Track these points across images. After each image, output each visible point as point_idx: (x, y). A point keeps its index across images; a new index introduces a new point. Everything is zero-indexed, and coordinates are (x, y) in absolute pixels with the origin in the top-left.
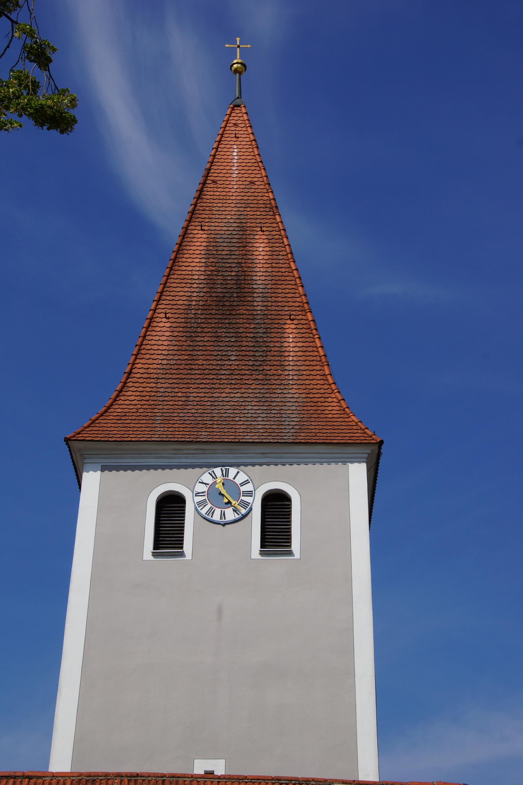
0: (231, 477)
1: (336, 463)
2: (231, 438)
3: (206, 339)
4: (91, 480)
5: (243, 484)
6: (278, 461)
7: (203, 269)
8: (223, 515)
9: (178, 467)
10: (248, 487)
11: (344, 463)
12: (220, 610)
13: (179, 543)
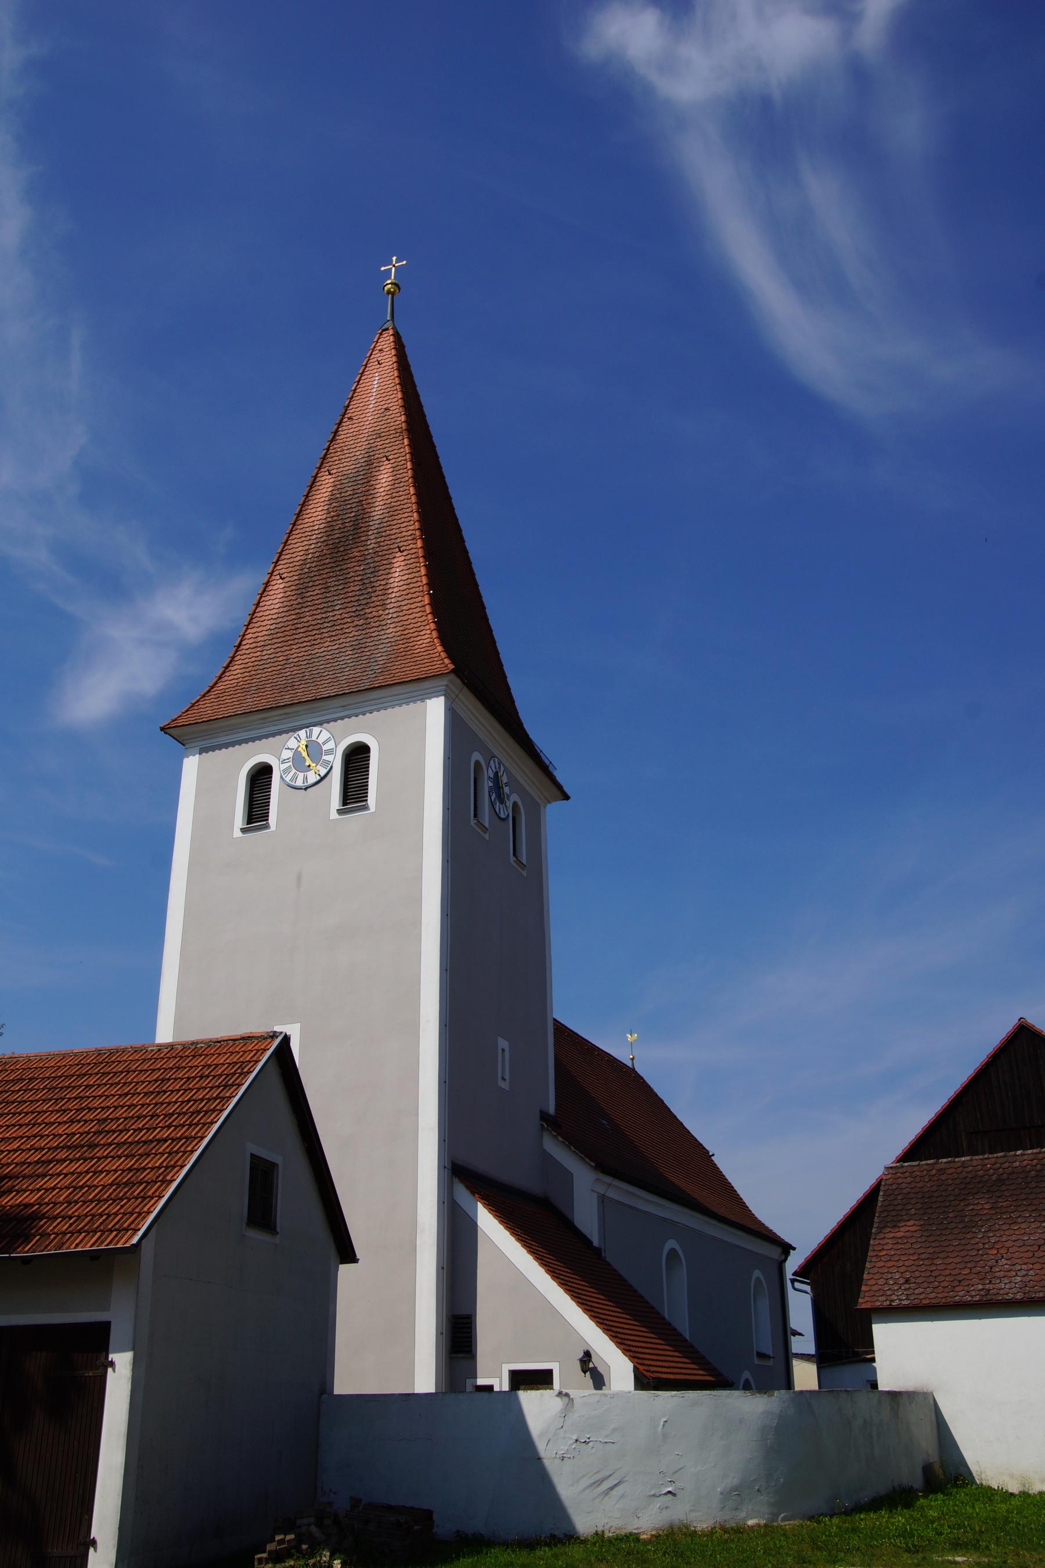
0: (314, 738)
1: (415, 702)
2: (310, 697)
3: (315, 593)
4: (191, 765)
5: (324, 743)
6: (357, 711)
7: (324, 517)
8: (306, 779)
9: (267, 737)
10: (331, 745)
11: (423, 700)
12: (299, 878)
13: (265, 816)
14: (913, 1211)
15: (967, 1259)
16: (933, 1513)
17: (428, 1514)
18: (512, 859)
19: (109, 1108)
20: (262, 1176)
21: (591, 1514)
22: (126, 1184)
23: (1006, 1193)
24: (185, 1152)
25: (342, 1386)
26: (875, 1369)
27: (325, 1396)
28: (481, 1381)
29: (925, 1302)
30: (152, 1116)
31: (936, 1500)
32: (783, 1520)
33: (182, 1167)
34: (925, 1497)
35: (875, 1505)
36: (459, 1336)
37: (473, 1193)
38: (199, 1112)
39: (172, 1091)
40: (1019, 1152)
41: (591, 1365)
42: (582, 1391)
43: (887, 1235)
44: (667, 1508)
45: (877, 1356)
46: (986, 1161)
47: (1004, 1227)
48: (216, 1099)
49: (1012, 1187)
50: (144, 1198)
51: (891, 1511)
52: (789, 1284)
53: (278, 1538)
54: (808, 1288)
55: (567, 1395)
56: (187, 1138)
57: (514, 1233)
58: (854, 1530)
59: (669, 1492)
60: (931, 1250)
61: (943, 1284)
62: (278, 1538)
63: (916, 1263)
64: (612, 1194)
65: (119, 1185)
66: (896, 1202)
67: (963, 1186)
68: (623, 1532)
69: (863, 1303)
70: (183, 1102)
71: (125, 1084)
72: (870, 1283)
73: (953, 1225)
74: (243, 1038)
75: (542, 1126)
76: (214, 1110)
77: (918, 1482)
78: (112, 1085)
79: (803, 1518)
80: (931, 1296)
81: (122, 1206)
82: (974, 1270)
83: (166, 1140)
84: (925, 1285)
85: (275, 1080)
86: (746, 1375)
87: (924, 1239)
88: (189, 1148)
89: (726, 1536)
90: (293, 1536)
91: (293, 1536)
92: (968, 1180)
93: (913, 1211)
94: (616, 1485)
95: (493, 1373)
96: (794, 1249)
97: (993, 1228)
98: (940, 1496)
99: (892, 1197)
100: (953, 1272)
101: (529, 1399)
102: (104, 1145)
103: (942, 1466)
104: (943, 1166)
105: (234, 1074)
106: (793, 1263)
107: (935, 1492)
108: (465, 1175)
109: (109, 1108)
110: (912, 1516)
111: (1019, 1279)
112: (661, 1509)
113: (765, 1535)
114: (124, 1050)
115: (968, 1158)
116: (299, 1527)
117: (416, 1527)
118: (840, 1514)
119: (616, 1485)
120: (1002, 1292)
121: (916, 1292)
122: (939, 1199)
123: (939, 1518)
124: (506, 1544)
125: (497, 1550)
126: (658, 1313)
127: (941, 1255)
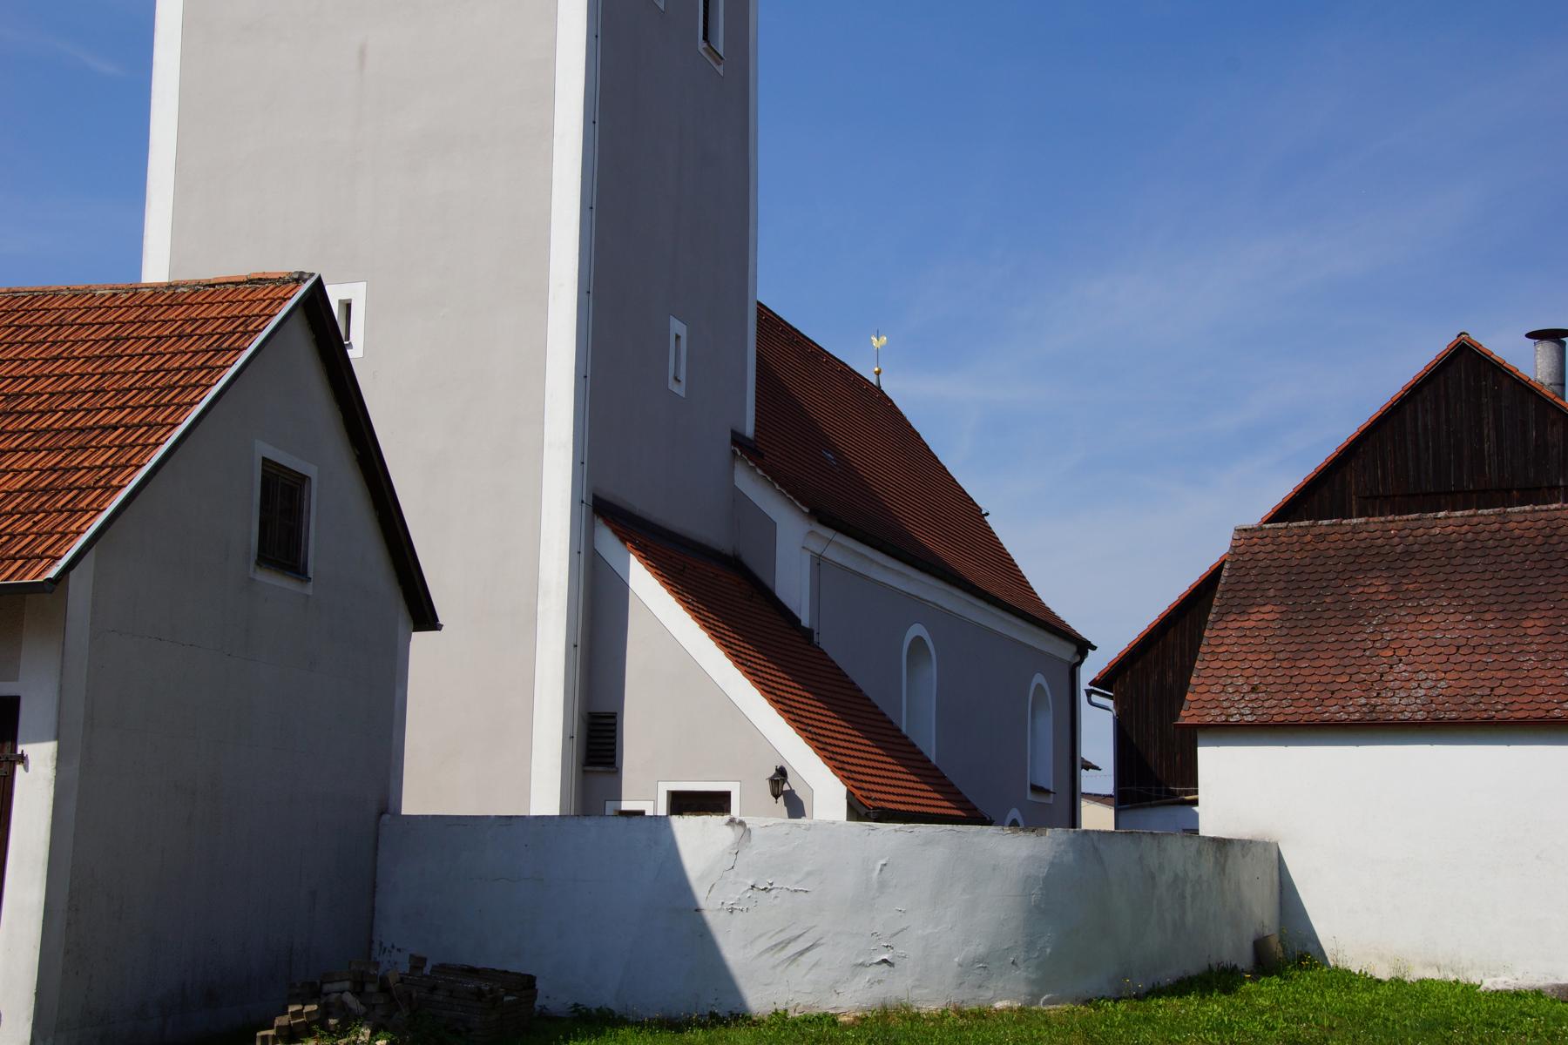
12: (362, 53)
14: (1271, 593)
15: (1346, 662)
16: (1263, 1002)
17: (528, 982)
18: (701, 45)
19: (24, 377)
20: (283, 498)
21: (768, 987)
22: (45, 490)
23: (1415, 572)
24: (145, 446)
25: (416, 800)
26: (1196, 815)
27: (386, 817)
28: (626, 805)
29: (1277, 718)
30: (96, 392)
31: (1269, 984)
32: (1047, 1003)
33: (139, 467)
34: (1254, 979)
35: (1181, 987)
36: (597, 742)
37: (624, 540)
38: (172, 387)
39: (131, 357)
40: (1441, 514)
41: (786, 787)
42: (764, 816)
43: (1231, 625)
44: (879, 982)
45: (1201, 796)
46: (1390, 526)
47: (1407, 619)
48: (200, 369)
49: (1425, 564)
50: (73, 512)
51: (1203, 997)
52: (1083, 697)
53: (292, 1009)
54: (1110, 703)
55: (742, 823)
56: (150, 426)
57: (682, 600)
58: (1147, 1020)
59: (885, 961)
60: (1293, 647)
61: (1306, 695)
62: (292, 1009)
63: (1270, 665)
64: (833, 554)
65: (33, 492)
66: (1247, 579)
67: (1351, 559)
68: (814, 1012)
69: (1187, 717)
70: (147, 372)
71: (54, 343)
72: (1199, 689)
73: (1331, 614)
74: (251, 281)
75: (734, 453)
76: (195, 386)
77: (1245, 960)
78: (32, 344)
79: (1075, 1001)
80: (1288, 713)
81: (35, 523)
82: (1355, 678)
83: (115, 428)
84: (1280, 695)
85: (301, 343)
86: (1014, 813)
87: (1285, 631)
88: (152, 440)
89: (961, 1022)
90: (315, 1007)
91: (315, 1007)
92: (1359, 551)
93: (1271, 593)
94: (808, 949)
95: (643, 792)
96: (1094, 648)
97: (1390, 620)
98: (1276, 980)
99: (1242, 572)
100: (1323, 679)
101: (690, 831)
102: (13, 432)
103: (1281, 941)
104: (1323, 530)
105: (233, 333)
106: (1091, 669)
107: (1269, 974)
108: (613, 514)
109: (24, 377)
110: (1232, 1005)
111: (1422, 692)
112: (871, 983)
113: (1019, 1022)
114: (55, 294)
115: (1363, 520)
116: (327, 994)
117: (507, 999)
118: (1129, 998)
119: (808, 949)
120: (1394, 709)
121: (1266, 704)
122: (1313, 577)
123: (1272, 1009)
124: (640, 1025)
125: (627, 1030)
126: (891, 722)
127: (1308, 655)
